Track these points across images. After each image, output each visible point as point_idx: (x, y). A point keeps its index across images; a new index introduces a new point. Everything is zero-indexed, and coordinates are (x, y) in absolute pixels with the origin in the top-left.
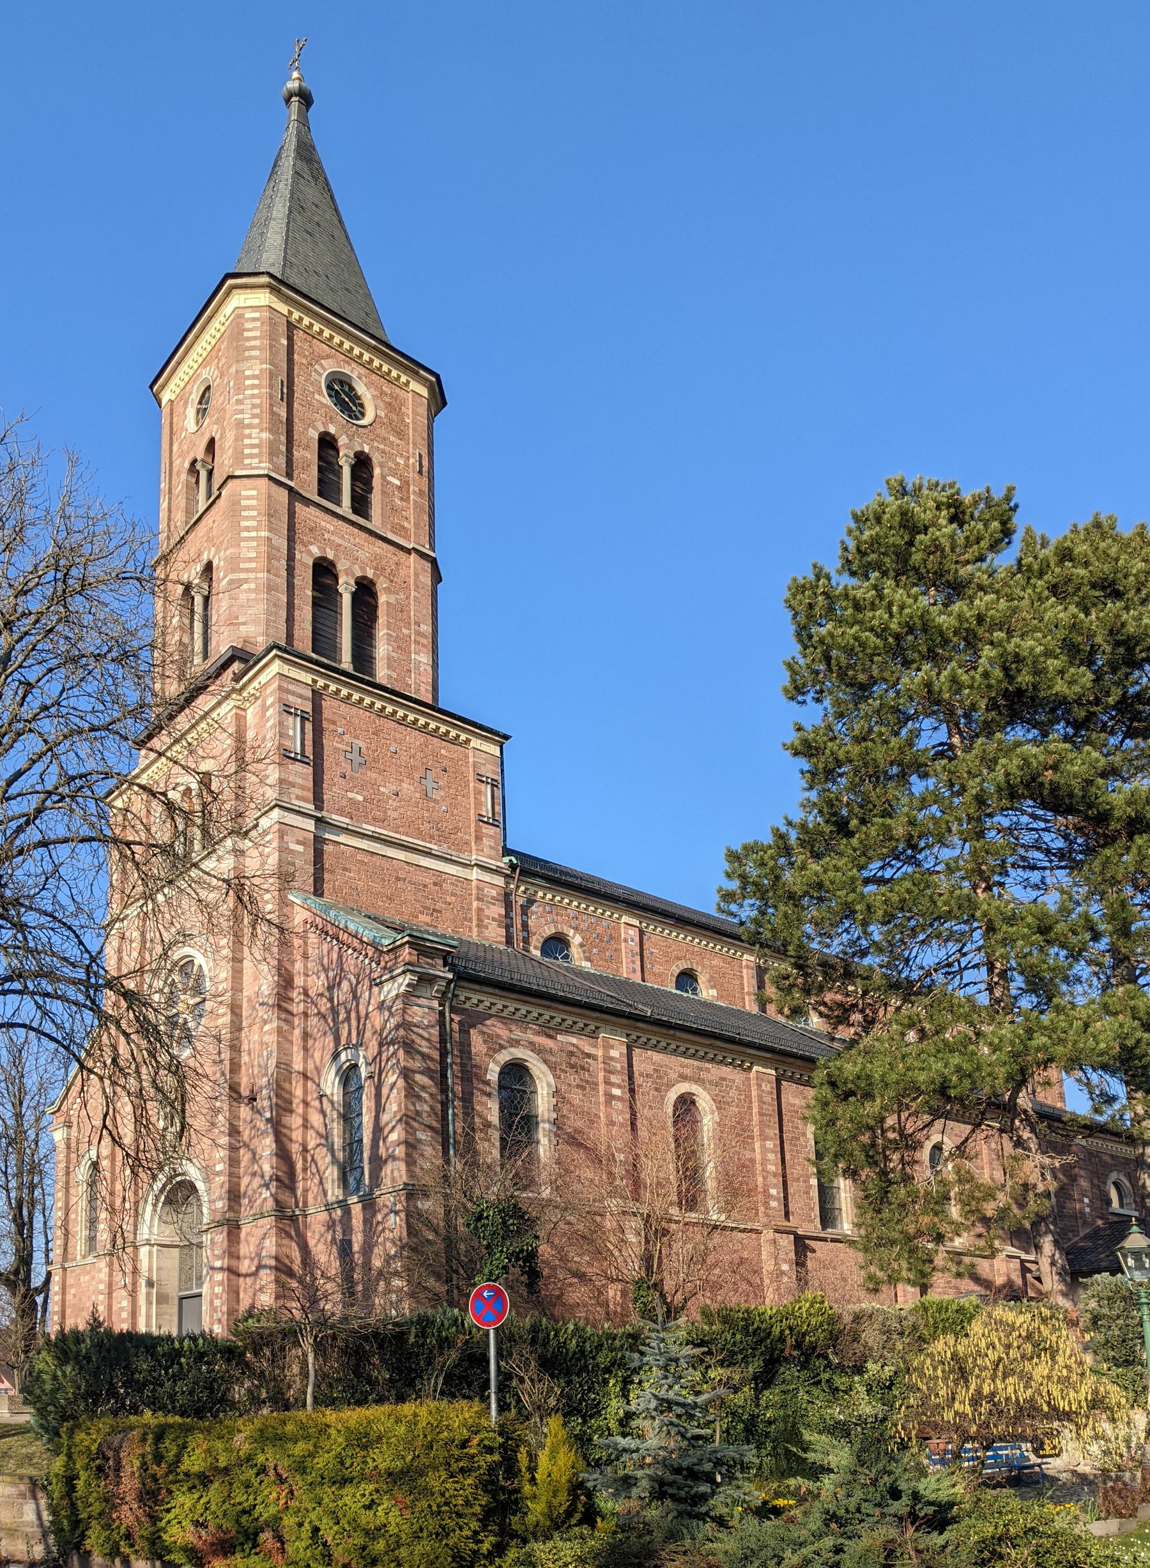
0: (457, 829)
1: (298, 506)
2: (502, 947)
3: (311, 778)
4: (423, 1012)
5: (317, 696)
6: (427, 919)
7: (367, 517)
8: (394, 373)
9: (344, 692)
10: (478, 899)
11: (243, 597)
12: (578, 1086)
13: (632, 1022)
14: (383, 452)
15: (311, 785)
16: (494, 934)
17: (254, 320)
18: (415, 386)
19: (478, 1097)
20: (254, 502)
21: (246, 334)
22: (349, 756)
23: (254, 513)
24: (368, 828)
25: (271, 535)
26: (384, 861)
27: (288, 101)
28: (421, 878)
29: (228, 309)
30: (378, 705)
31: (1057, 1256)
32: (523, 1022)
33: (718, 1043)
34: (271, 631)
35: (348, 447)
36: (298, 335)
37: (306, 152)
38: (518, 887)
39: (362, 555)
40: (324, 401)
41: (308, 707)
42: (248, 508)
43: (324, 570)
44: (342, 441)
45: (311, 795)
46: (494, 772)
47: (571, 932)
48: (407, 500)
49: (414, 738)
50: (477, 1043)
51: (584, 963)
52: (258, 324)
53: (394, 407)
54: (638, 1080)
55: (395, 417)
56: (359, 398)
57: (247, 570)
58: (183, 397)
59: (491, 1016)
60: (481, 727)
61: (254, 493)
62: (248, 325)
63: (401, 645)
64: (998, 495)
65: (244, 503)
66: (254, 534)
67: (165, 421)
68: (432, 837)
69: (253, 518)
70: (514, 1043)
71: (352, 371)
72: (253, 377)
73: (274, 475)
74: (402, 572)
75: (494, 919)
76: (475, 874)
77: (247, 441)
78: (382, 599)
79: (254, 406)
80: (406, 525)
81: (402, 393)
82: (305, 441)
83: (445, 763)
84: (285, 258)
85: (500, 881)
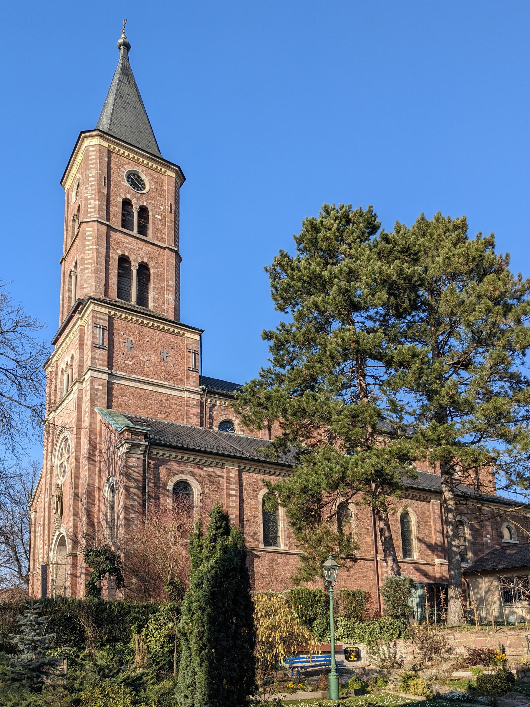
0: (178, 375)
1: (112, 233)
2: (197, 427)
3: (107, 356)
4: (136, 461)
5: (111, 319)
6: (162, 416)
7: (146, 235)
8: (159, 168)
9: (124, 316)
10: (187, 406)
11: (86, 275)
12: (213, 491)
13: (240, 460)
14: (153, 204)
15: (106, 359)
16: (194, 421)
17: (93, 151)
18: (169, 173)
19: (162, 497)
20: (91, 233)
21: (90, 158)
22: (126, 344)
23: (91, 238)
24: (134, 376)
25: (98, 247)
26: (141, 392)
27: (119, 48)
28: (159, 398)
29: (83, 147)
30: (140, 320)
31: (394, 566)
32: (187, 462)
33: (285, 468)
34: (97, 290)
35: (136, 204)
36: (113, 156)
37: (126, 71)
38: (206, 400)
39: (142, 252)
40: (125, 184)
41: (106, 324)
42: (89, 236)
43: (124, 261)
44: (134, 201)
45: (106, 363)
46: (196, 347)
47: (234, 419)
48: (165, 225)
49: (158, 334)
50: (163, 472)
51: (240, 433)
52: (95, 153)
53: (159, 183)
54: (245, 486)
55: (159, 188)
56: (142, 181)
57: (88, 264)
58: (72, 187)
59: (170, 461)
60: (189, 327)
61: (91, 229)
62: (91, 154)
63: (160, 292)
64: (365, 210)
65: (87, 234)
66: (91, 247)
67: (66, 198)
68: (165, 379)
69: (91, 240)
70: (183, 472)
71: (139, 169)
72: (92, 177)
73: (99, 220)
74: (161, 258)
75: (194, 415)
76: (186, 394)
77: (89, 206)
78: (152, 271)
79: (92, 190)
80: (164, 236)
81: (163, 177)
82: (115, 203)
83: (173, 344)
84: (111, 121)
85: (198, 397)
